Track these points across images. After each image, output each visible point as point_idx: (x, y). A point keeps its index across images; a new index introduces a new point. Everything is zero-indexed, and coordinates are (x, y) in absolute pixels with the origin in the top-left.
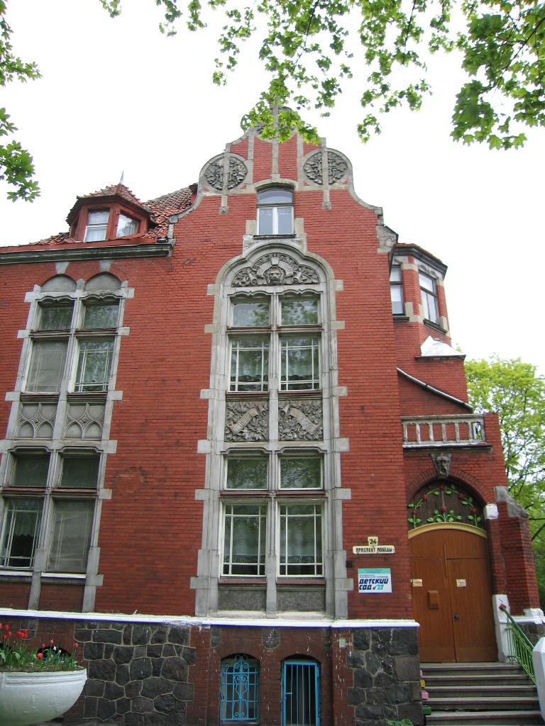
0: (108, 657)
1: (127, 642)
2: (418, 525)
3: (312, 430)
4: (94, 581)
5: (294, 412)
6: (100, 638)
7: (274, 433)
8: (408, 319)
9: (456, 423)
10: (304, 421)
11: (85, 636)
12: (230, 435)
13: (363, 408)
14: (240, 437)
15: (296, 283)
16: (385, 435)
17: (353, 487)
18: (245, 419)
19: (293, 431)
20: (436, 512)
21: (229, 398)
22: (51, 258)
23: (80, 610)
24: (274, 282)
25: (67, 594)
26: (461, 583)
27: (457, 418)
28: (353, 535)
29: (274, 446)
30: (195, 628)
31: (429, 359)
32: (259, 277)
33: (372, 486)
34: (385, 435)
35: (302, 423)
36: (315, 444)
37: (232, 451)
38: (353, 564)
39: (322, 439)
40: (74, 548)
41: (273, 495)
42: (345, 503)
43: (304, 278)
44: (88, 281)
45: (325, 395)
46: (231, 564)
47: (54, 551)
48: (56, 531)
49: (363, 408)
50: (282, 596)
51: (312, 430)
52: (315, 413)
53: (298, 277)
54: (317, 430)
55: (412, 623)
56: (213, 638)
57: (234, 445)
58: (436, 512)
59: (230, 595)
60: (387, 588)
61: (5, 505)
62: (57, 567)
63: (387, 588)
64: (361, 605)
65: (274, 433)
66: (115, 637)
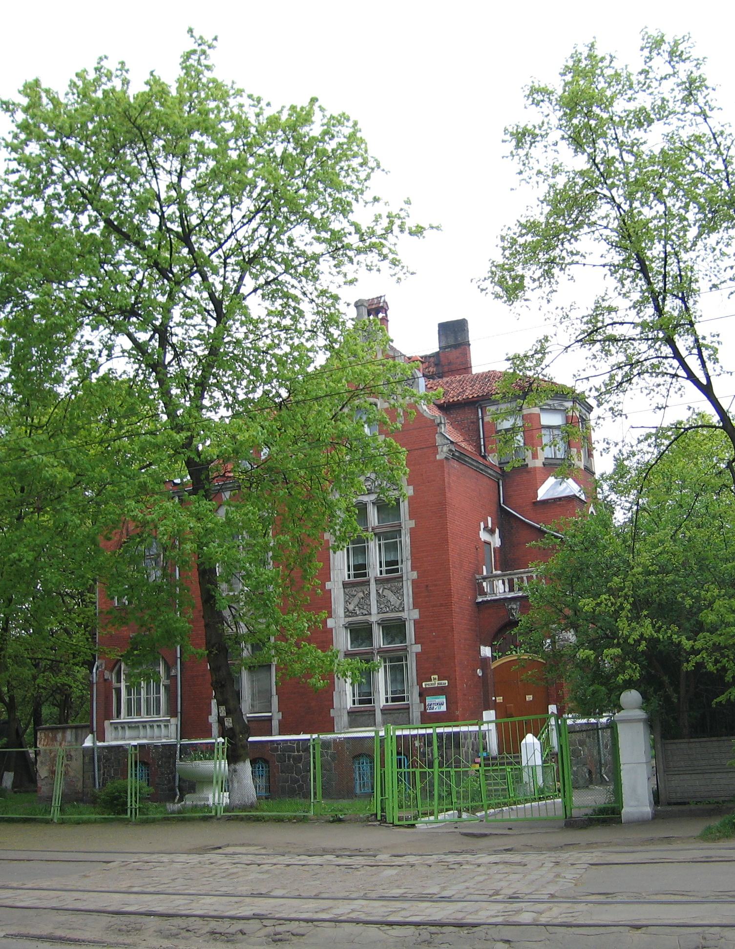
0: (289, 761)
1: (298, 751)
2: (499, 657)
3: (397, 605)
4: (277, 717)
5: (386, 592)
6: (284, 750)
7: (374, 609)
8: (527, 465)
9: (525, 576)
10: (392, 598)
11: (276, 749)
12: (348, 613)
13: (427, 586)
14: (352, 614)
16: (441, 605)
17: (422, 644)
18: (356, 601)
19: (386, 606)
20: (512, 647)
21: (345, 585)
23: (271, 735)
26: (529, 698)
27: (524, 573)
28: (423, 676)
29: (374, 618)
30: (335, 740)
31: (545, 502)
33: (434, 642)
34: (441, 605)
36: (400, 614)
37: (350, 624)
38: (423, 694)
39: (403, 610)
40: (262, 696)
41: (375, 652)
42: (417, 654)
45: (404, 578)
46: (389, 696)
47: (253, 699)
48: (252, 687)
49: (427, 586)
50: (385, 716)
51: (397, 605)
52: (398, 592)
54: (401, 604)
55: (251, 739)
56: (346, 745)
57: (350, 619)
58: (512, 647)
59: (357, 717)
60: (444, 708)
62: (256, 710)
63: (444, 708)
64: (428, 718)
65: (374, 609)
66: (292, 749)
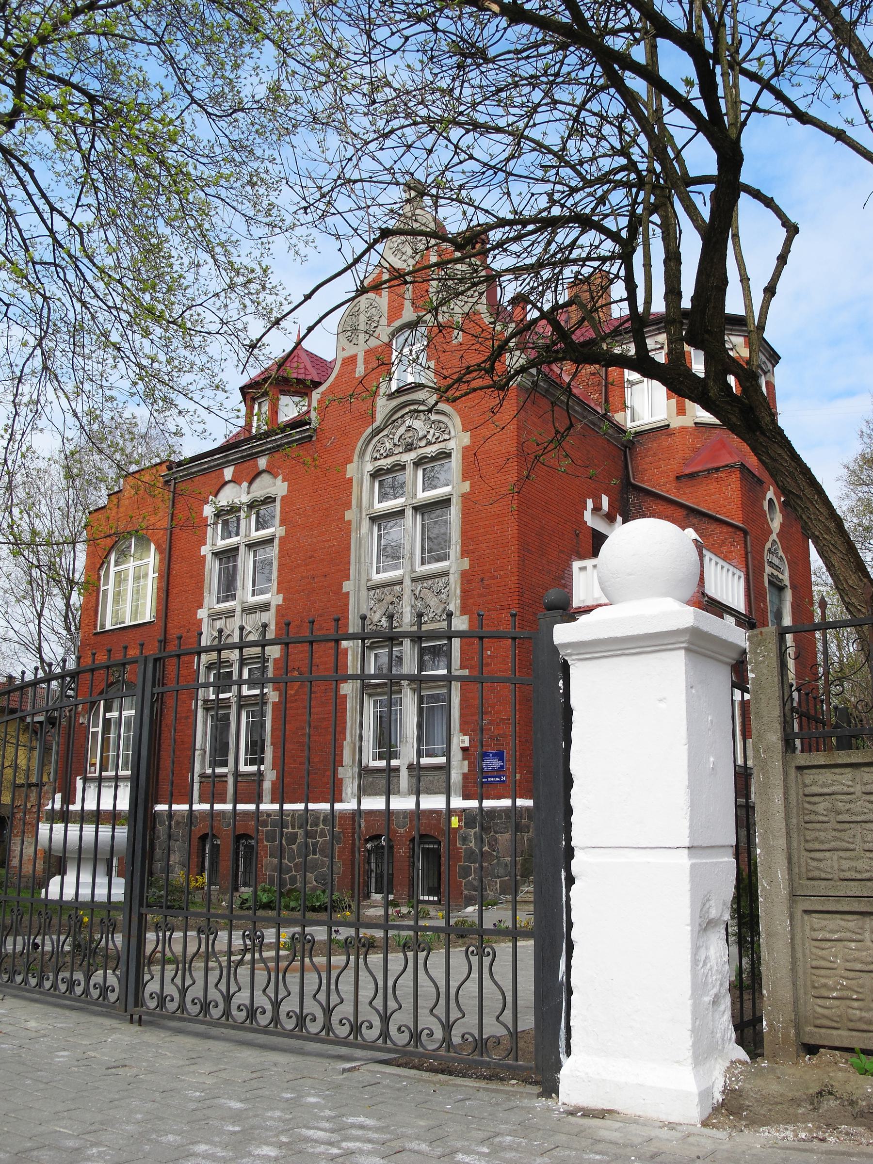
15: (429, 443)
22: (218, 465)
24: (409, 448)
25: (250, 789)
32: (395, 445)
35: (432, 604)
43: (437, 435)
44: (250, 483)
53: (429, 437)
61: (464, 759)
